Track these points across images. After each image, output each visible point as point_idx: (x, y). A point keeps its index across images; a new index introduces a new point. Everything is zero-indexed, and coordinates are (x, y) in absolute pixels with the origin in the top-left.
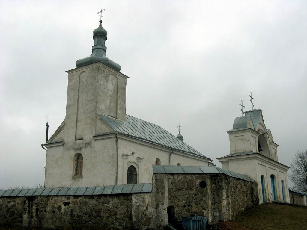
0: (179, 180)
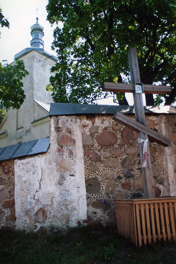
0: (106, 129)
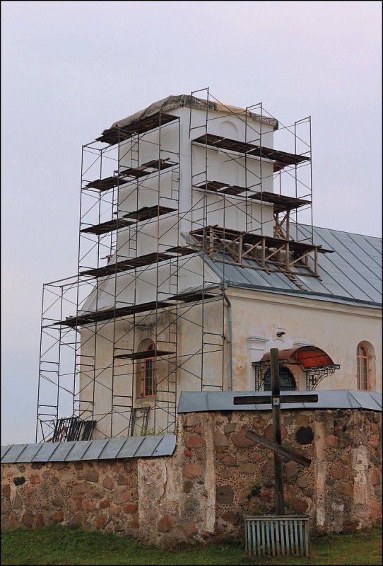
0: (244, 427)
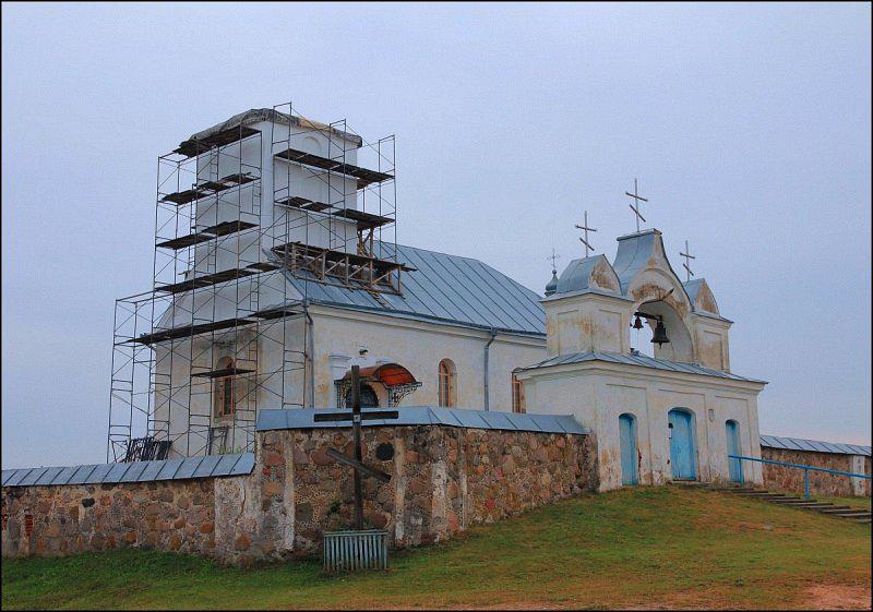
0: (325, 444)
